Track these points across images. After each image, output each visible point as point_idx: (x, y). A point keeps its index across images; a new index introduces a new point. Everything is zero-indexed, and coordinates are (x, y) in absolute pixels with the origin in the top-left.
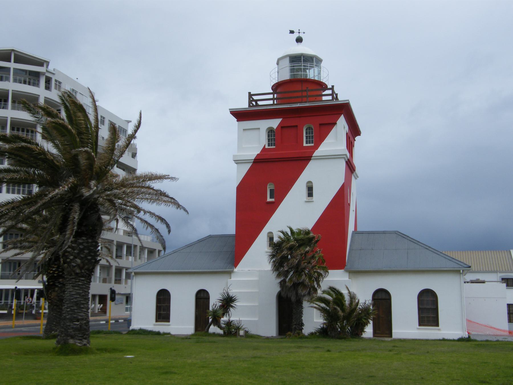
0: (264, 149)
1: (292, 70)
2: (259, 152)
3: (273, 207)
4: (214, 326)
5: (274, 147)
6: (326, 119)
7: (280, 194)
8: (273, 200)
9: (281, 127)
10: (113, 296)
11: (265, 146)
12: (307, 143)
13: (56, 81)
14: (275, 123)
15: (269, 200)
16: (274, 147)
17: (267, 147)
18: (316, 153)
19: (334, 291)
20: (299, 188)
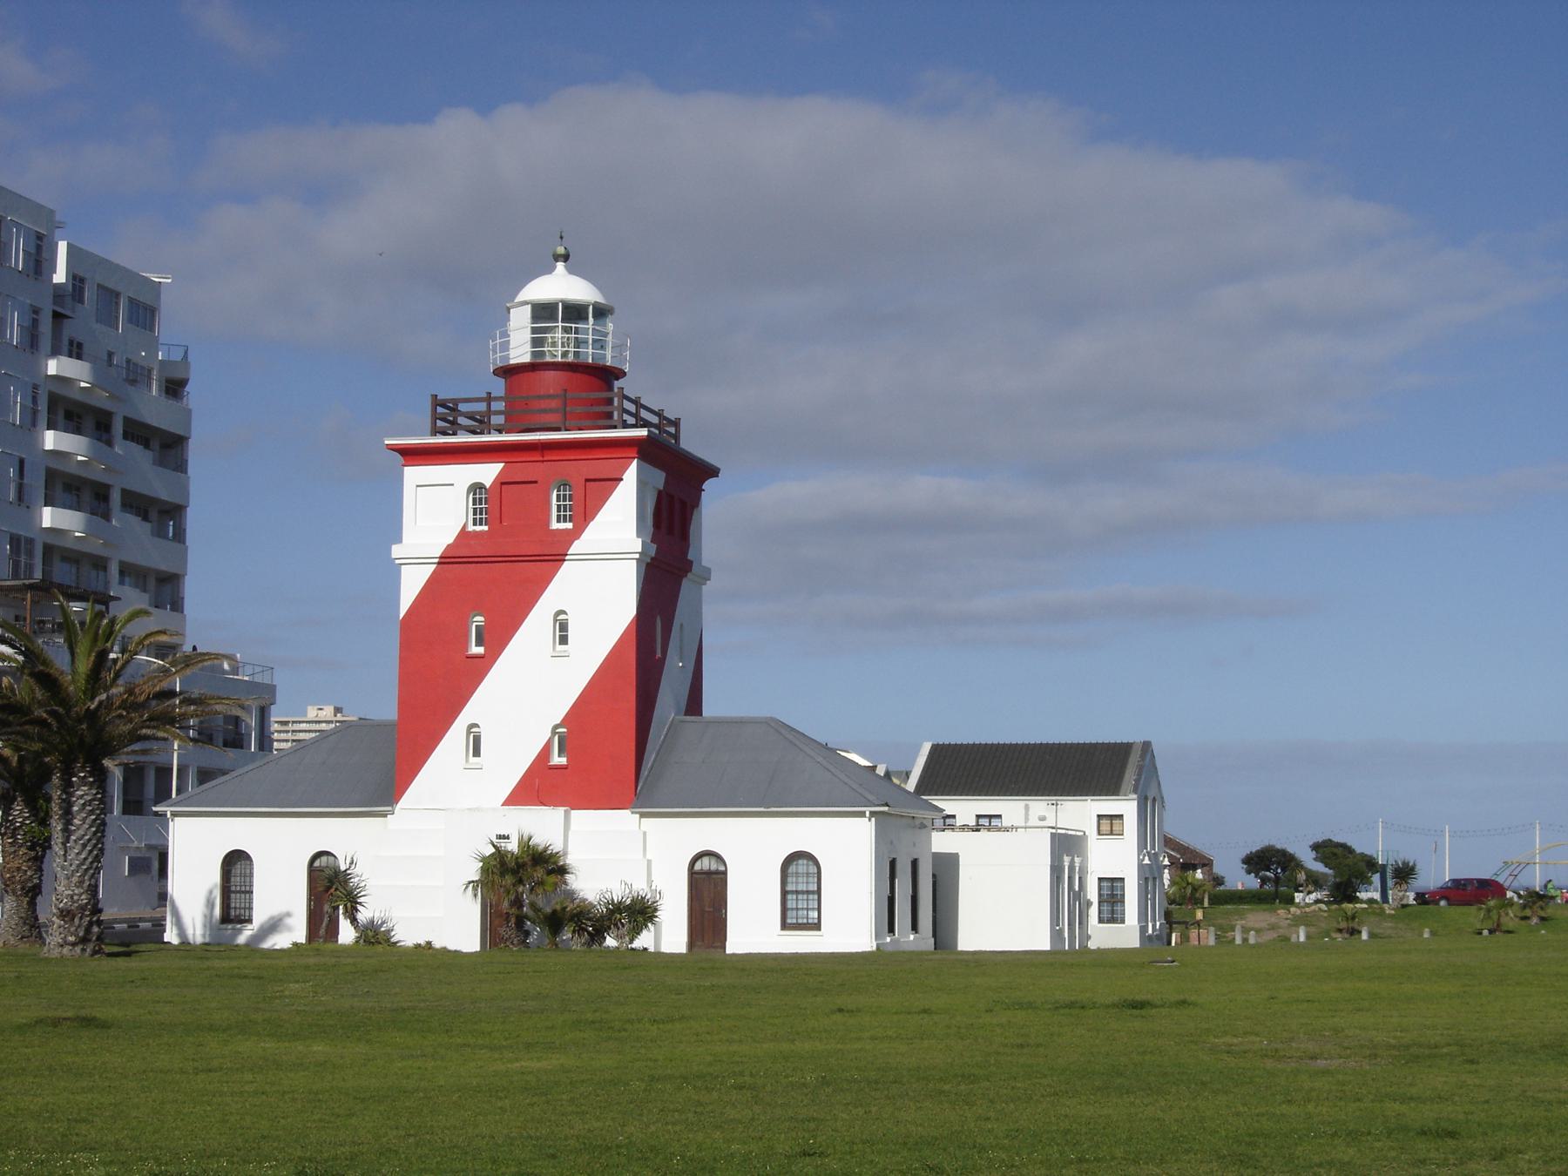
0: (463, 533)
1: (536, 342)
2: (451, 540)
3: (478, 670)
4: (295, 944)
5: (486, 528)
6: (601, 467)
7: (497, 638)
8: (480, 650)
9: (502, 482)
10: (155, 444)
11: (465, 526)
12: (559, 521)
13: (131, 300)
14: (487, 473)
15: (555, 525)
16: (486, 528)
17: (471, 528)
18: (576, 547)
19: (1143, 756)
20: (536, 625)
